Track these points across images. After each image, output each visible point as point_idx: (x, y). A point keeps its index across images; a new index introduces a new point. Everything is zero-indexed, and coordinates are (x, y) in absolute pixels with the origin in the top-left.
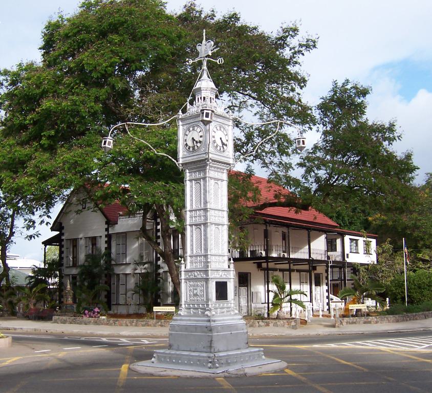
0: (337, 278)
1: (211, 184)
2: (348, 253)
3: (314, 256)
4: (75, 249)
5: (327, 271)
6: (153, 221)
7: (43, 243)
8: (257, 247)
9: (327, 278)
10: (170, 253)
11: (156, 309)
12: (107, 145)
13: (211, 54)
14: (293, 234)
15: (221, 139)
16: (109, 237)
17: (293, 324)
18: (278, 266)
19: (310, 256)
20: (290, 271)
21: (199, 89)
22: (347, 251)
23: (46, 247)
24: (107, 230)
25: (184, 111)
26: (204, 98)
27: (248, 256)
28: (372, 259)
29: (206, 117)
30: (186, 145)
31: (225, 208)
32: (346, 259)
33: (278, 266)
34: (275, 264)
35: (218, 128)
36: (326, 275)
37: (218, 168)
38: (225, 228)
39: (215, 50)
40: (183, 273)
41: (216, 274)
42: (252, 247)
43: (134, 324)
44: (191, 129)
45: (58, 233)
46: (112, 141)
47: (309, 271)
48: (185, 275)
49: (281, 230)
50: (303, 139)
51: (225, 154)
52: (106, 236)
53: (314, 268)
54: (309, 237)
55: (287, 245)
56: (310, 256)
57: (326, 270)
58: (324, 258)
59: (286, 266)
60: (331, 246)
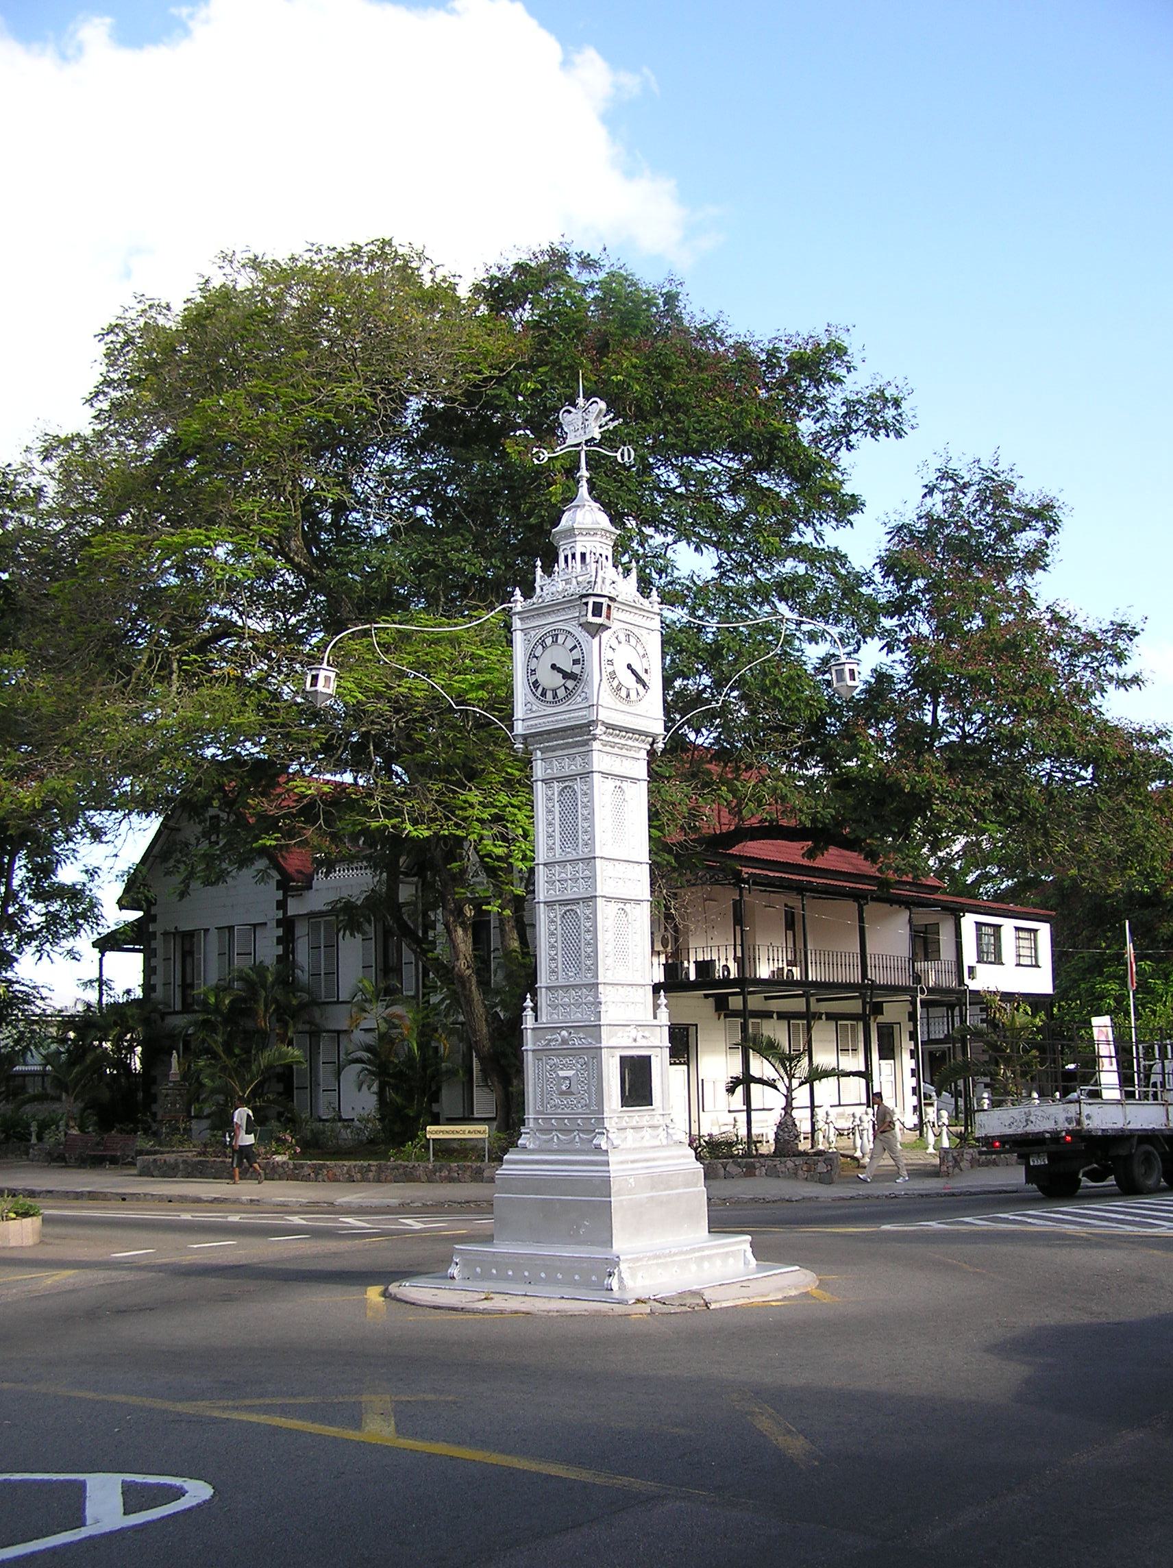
0: (942, 1037)
1: (602, 789)
2: (973, 964)
3: (878, 976)
4: (189, 960)
5: (912, 1017)
6: (415, 879)
7: (95, 945)
8: (715, 950)
9: (913, 1036)
10: (468, 972)
11: (434, 1132)
12: (320, 687)
13: (598, 437)
14: (817, 912)
15: (629, 666)
16: (287, 924)
17: (821, 1167)
18: (775, 1005)
19: (864, 975)
20: (809, 1017)
21: (570, 533)
22: (970, 957)
23: (103, 955)
24: (282, 905)
25: (528, 593)
26: (583, 555)
27: (687, 974)
28: (1041, 981)
29: (594, 615)
30: (536, 684)
31: (644, 856)
32: (967, 980)
33: (775, 1005)
34: (767, 998)
35: (622, 638)
36: (910, 1026)
37: (623, 747)
38: (646, 909)
39: (611, 426)
40: (529, 1035)
41: (620, 1034)
42: (700, 951)
43: (371, 1175)
44: (549, 641)
45: (140, 914)
46: (333, 675)
47: (863, 1018)
48: (536, 1040)
49: (781, 900)
50: (852, 667)
51: (639, 708)
52: (279, 923)
53: (878, 1009)
54: (861, 920)
55: (800, 945)
56: (864, 975)
57: (909, 1013)
58: (904, 980)
59: (799, 1005)
60: (923, 944)
